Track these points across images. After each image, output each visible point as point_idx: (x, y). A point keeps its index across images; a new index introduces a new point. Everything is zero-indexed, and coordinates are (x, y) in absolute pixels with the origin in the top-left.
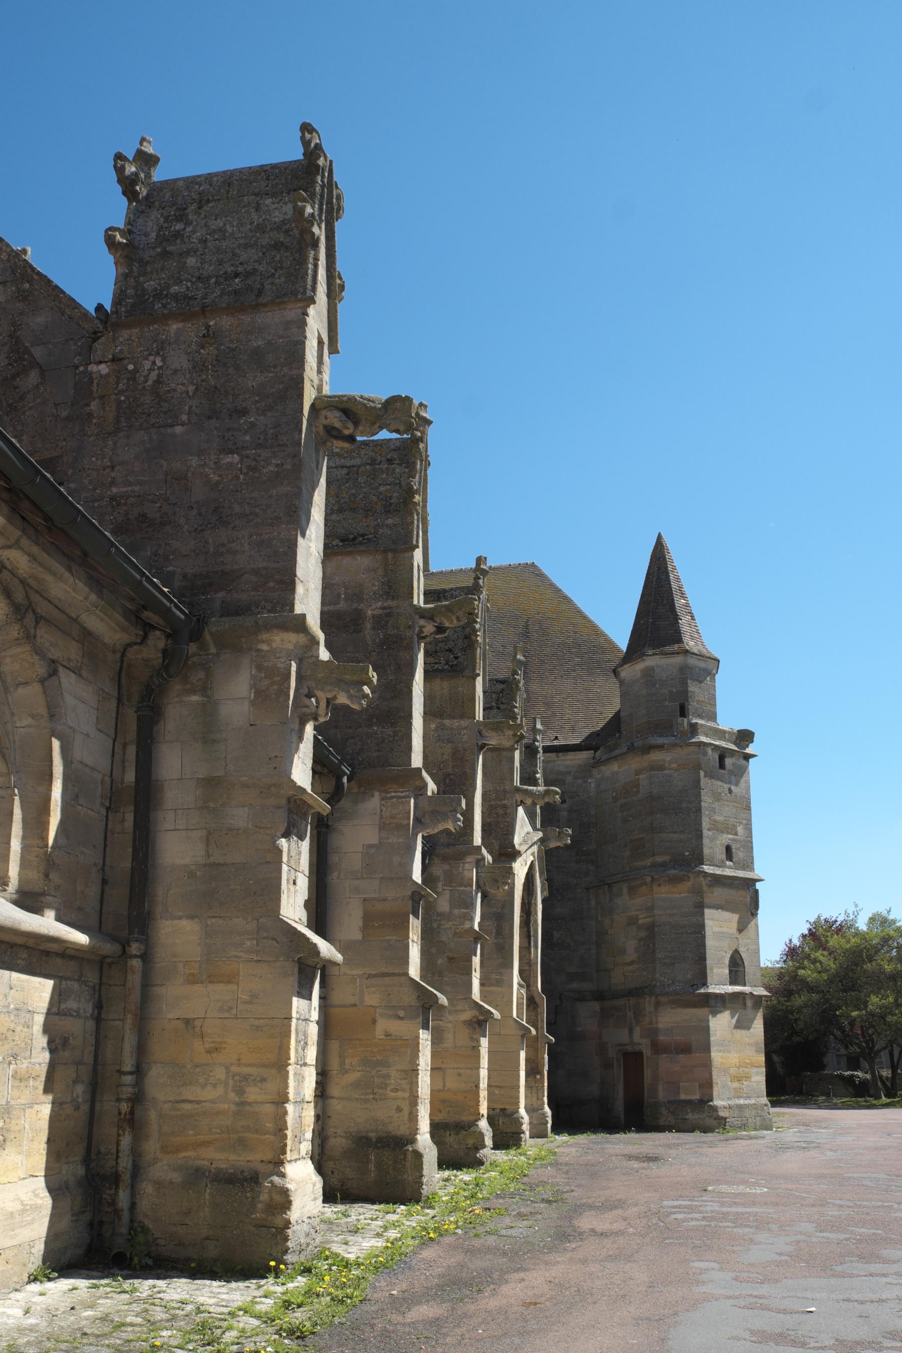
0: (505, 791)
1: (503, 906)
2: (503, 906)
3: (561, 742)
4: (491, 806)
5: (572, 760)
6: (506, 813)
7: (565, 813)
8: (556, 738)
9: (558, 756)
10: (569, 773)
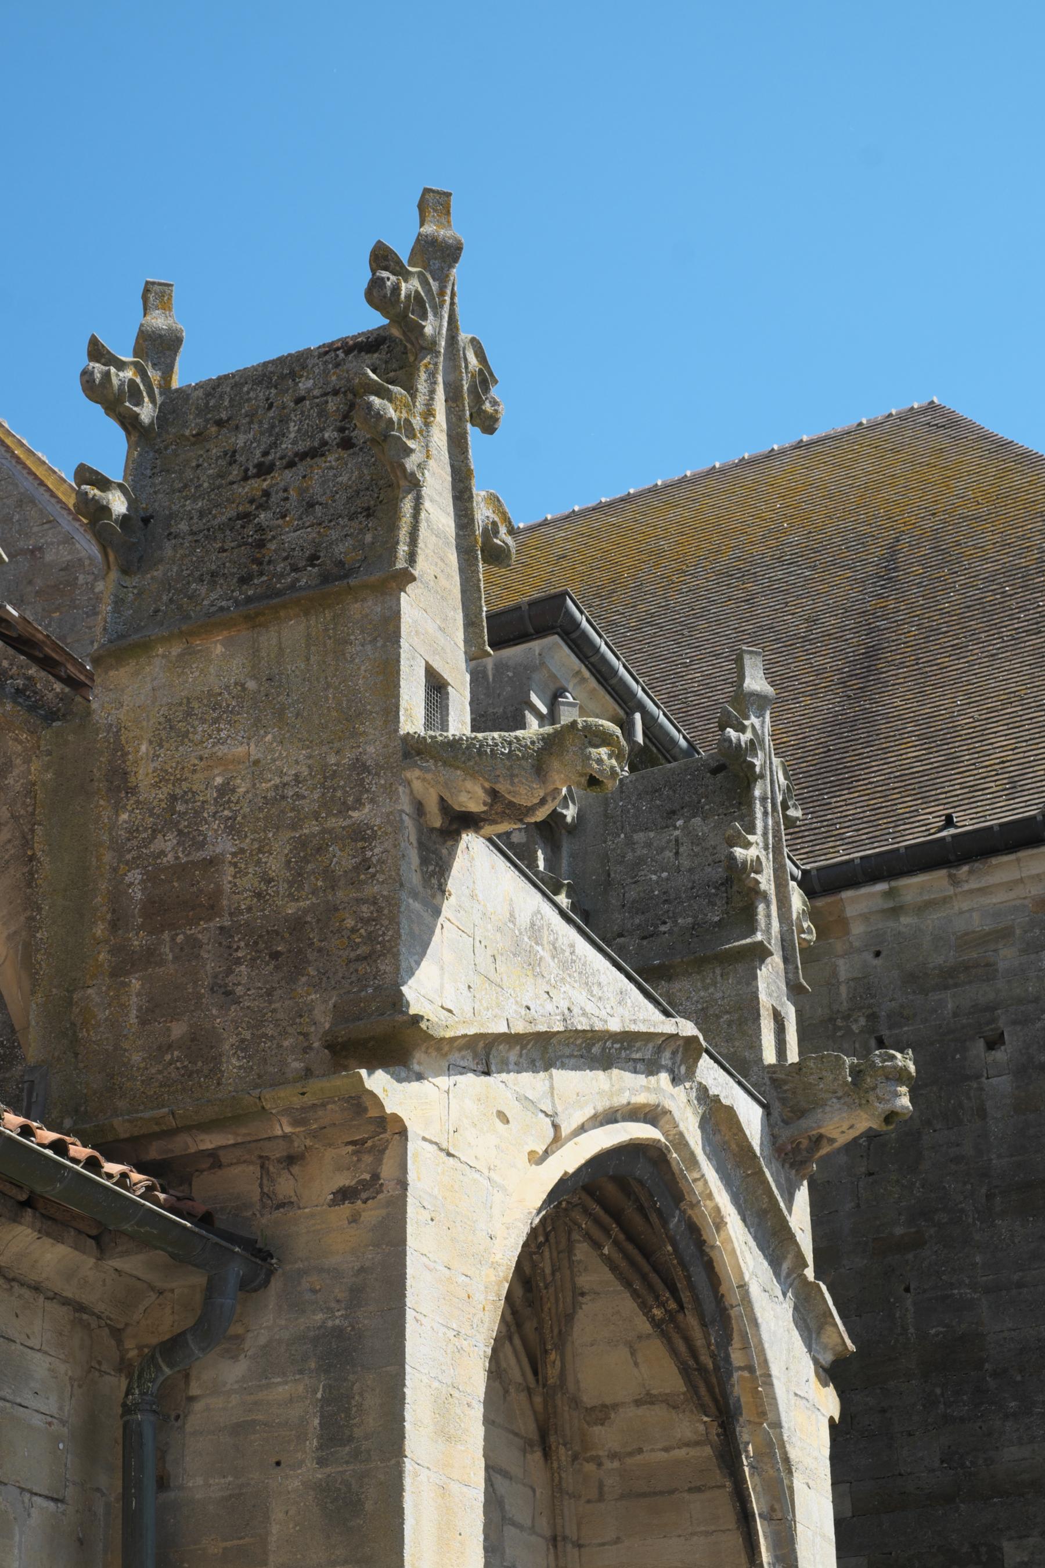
0: (360, 766)
1: (356, 1295)
2: (356, 1295)
3: (966, 823)
4: (302, 843)
5: (1010, 886)
6: (365, 864)
7: (1002, 1084)
8: (949, 822)
9: (955, 881)
10: (1004, 934)
